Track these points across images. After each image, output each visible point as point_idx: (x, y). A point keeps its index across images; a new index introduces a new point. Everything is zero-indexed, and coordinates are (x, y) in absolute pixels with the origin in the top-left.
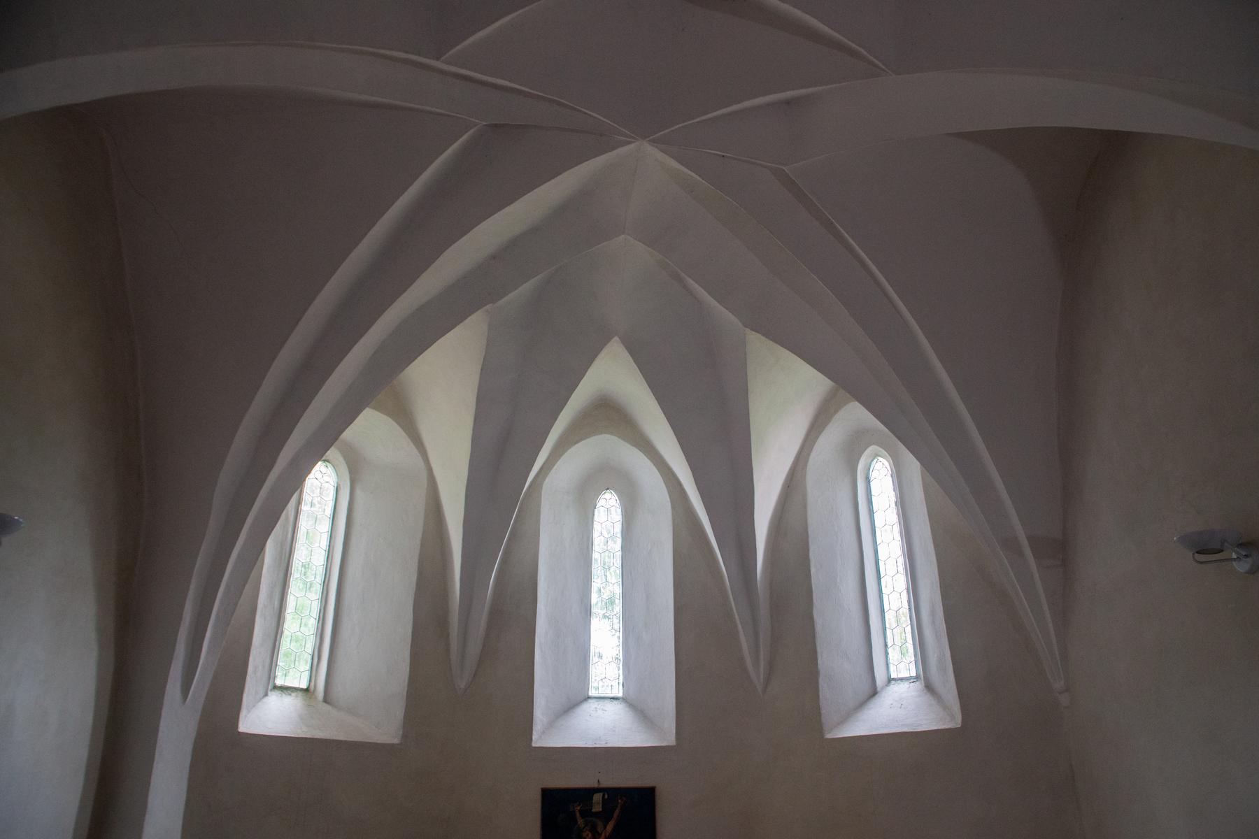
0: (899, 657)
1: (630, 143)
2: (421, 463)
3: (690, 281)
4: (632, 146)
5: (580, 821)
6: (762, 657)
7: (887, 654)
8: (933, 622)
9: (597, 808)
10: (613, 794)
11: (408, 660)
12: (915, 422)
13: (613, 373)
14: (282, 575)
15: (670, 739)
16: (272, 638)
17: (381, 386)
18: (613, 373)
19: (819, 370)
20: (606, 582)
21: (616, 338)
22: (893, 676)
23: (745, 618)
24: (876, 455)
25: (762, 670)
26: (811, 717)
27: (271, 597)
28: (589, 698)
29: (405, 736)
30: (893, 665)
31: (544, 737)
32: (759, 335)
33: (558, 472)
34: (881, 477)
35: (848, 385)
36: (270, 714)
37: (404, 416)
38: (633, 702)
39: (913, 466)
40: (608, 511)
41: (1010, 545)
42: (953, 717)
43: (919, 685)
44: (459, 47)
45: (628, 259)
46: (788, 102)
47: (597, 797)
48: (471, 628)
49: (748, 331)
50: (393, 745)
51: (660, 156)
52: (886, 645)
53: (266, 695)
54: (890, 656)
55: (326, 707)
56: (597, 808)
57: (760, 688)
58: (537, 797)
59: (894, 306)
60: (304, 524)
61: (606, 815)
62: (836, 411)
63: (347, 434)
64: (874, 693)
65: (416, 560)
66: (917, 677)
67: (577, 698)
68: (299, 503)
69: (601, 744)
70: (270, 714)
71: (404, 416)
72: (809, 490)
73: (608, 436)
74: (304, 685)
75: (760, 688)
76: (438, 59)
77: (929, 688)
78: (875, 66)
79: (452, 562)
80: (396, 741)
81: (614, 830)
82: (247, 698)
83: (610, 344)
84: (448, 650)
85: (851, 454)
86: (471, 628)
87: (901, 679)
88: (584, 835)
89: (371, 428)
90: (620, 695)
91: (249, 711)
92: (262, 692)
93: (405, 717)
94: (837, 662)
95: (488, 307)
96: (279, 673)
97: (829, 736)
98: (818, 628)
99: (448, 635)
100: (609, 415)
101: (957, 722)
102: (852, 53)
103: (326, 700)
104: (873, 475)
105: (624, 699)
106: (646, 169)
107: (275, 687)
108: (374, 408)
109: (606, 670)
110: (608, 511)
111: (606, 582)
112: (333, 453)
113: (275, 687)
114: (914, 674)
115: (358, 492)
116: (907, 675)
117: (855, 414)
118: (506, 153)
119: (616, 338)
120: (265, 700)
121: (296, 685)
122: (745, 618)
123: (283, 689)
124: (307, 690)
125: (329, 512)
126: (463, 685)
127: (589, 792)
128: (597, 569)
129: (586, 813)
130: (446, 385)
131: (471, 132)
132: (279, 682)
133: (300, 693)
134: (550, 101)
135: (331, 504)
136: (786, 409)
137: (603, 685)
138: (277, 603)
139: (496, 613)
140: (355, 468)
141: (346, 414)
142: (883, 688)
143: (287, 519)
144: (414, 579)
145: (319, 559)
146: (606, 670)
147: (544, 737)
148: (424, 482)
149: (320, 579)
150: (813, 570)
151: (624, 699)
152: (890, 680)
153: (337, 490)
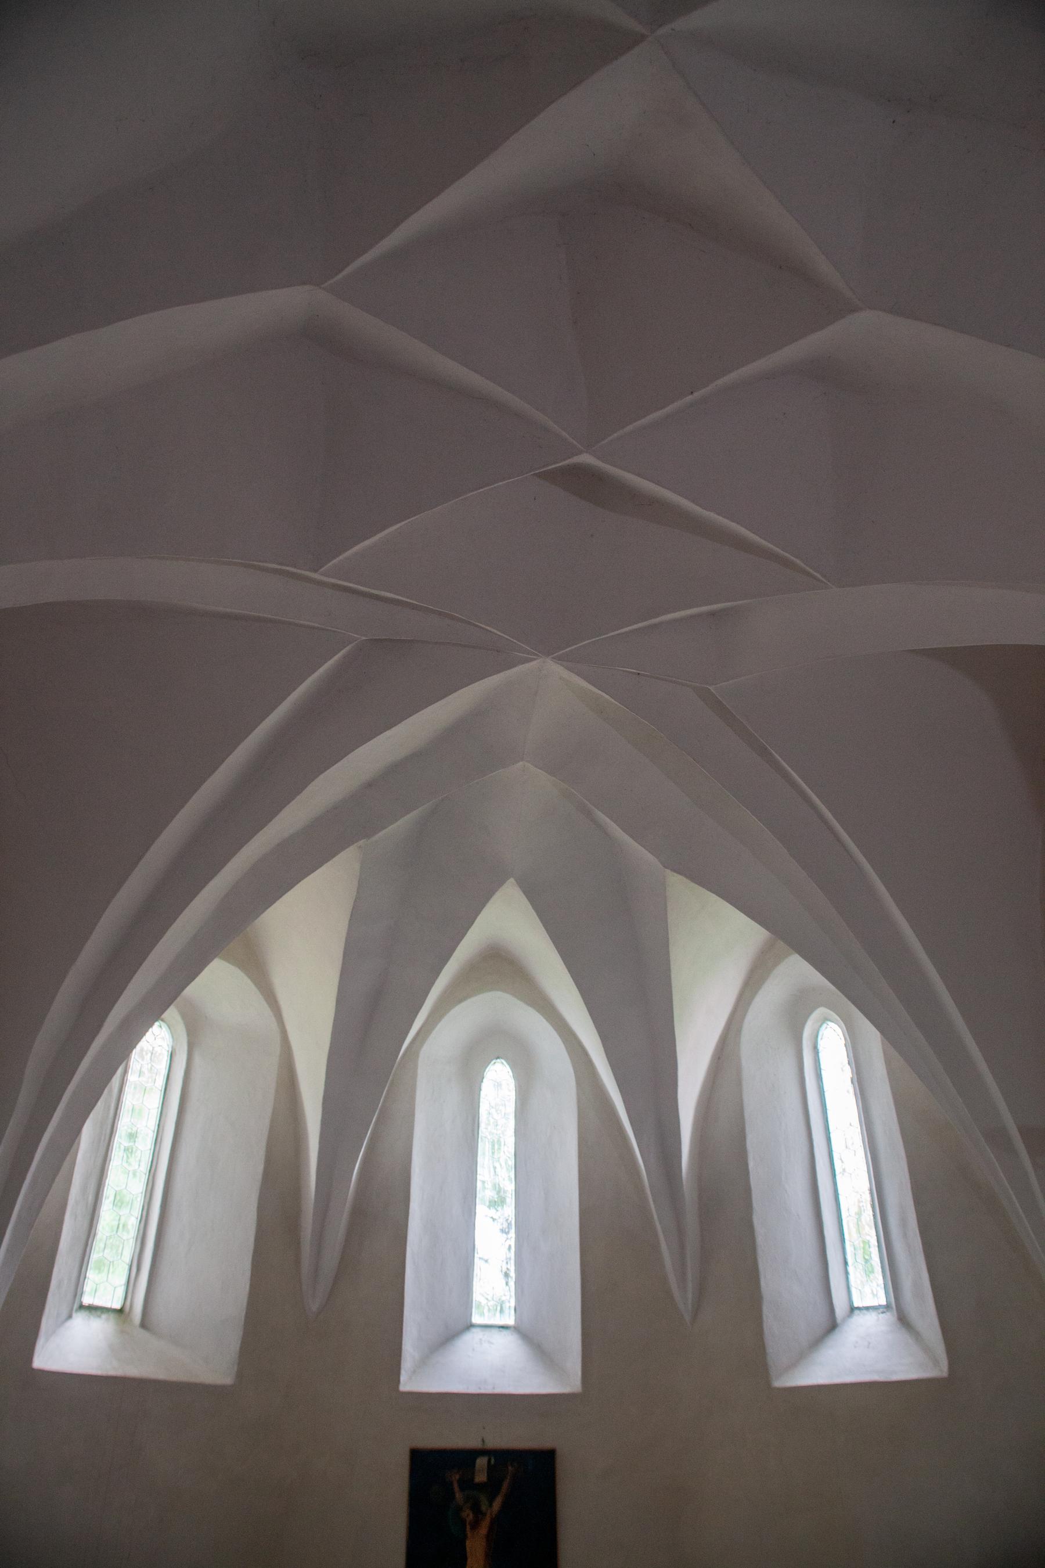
0: (865, 1284)
1: (532, 660)
2: (274, 1025)
3: (599, 814)
4: (535, 662)
5: (459, 1495)
6: (690, 1285)
7: (847, 1273)
8: (905, 1235)
9: (481, 1477)
10: (502, 1457)
11: (248, 1274)
12: (870, 979)
13: (508, 919)
14: (88, 1217)
15: (570, 1382)
16: (84, 1238)
17: (231, 933)
18: (508, 919)
19: (753, 918)
20: (496, 1169)
21: (512, 880)
22: (856, 1305)
23: (669, 1237)
24: (826, 1019)
25: (690, 1296)
26: (753, 1358)
27: (84, 1189)
28: (472, 1326)
29: (240, 1375)
30: (857, 1302)
31: (414, 1379)
32: (680, 877)
33: (438, 1040)
34: (831, 1043)
35: (785, 933)
36: (73, 1345)
37: (256, 967)
38: (524, 1332)
39: (872, 1037)
40: (498, 1082)
41: (997, 1137)
42: (936, 1362)
43: (890, 1317)
44: (335, 561)
45: (524, 798)
46: (713, 614)
47: (481, 1462)
48: (327, 1242)
49: (668, 871)
50: (223, 1387)
51: (566, 674)
52: (846, 1263)
53: (70, 1317)
54: (851, 1277)
55: (142, 1331)
56: (481, 1477)
57: (687, 1318)
58: (405, 1460)
59: (839, 840)
60: (129, 1099)
61: (492, 1487)
62: (776, 964)
63: (191, 991)
64: (832, 1326)
65: (264, 1144)
66: (888, 1307)
67: (456, 1327)
68: (125, 1072)
69: (487, 1389)
70: (73, 1345)
71: (256, 967)
72: (744, 1063)
73: (499, 993)
74: (117, 1305)
75: (687, 1318)
76: (316, 571)
77: (903, 1320)
78: (815, 578)
79: (307, 1148)
80: (228, 1380)
81: (504, 1505)
82: (47, 1322)
83: (504, 887)
84: (297, 1262)
85: (795, 1018)
86: (327, 1242)
87: (867, 1308)
88: (464, 1514)
89: (219, 984)
90: (511, 1322)
91: (47, 1340)
92: (65, 1313)
93: (241, 1348)
94: (784, 1285)
95: (361, 842)
96: (88, 1287)
97: (778, 1383)
98: (760, 1240)
99: (299, 1243)
100: (500, 967)
101: (940, 1369)
102: (786, 563)
103: (144, 1325)
104: (822, 1045)
105: (517, 1329)
106: (549, 691)
107: (82, 1307)
108: (225, 959)
109: (494, 1286)
110: (498, 1082)
111: (496, 1169)
112: (172, 1013)
113: (82, 1307)
114: (884, 1302)
115: (197, 1060)
116: (875, 1303)
117: (796, 971)
118: (383, 674)
119: (512, 880)
120: (69, 1323)
121: (108, 1305)
122: (669, 1237)
123: (92, 1309)
124: (120, 1311)
125: (160, 1082)
126: (314, 1306)
127: (471, 1455)
128: (484, 1148)
129: (467, 1484)
130: (308, 934)
131: (347, 648)
132: (87, 1300)
133: (112, 1315)
134: (440, 614)
135: (164, 1072)
136: (715, 964)
137: (491, 1313)
138: (91, 1198)
139: (359, 1213)
140: (195, 1030)
141: (190, 965)
142: (844, 1320)
143: (111, 1091)
144: (260, 1168)
145: (137, 1188)
146: (494, 1286)
147: (414, 1379)
148: (276, 1048)
149: (144, 1167)
150: (751, 1164)
151: (517, 1329)
152: (852, 1309)
153: (172, 1056)
